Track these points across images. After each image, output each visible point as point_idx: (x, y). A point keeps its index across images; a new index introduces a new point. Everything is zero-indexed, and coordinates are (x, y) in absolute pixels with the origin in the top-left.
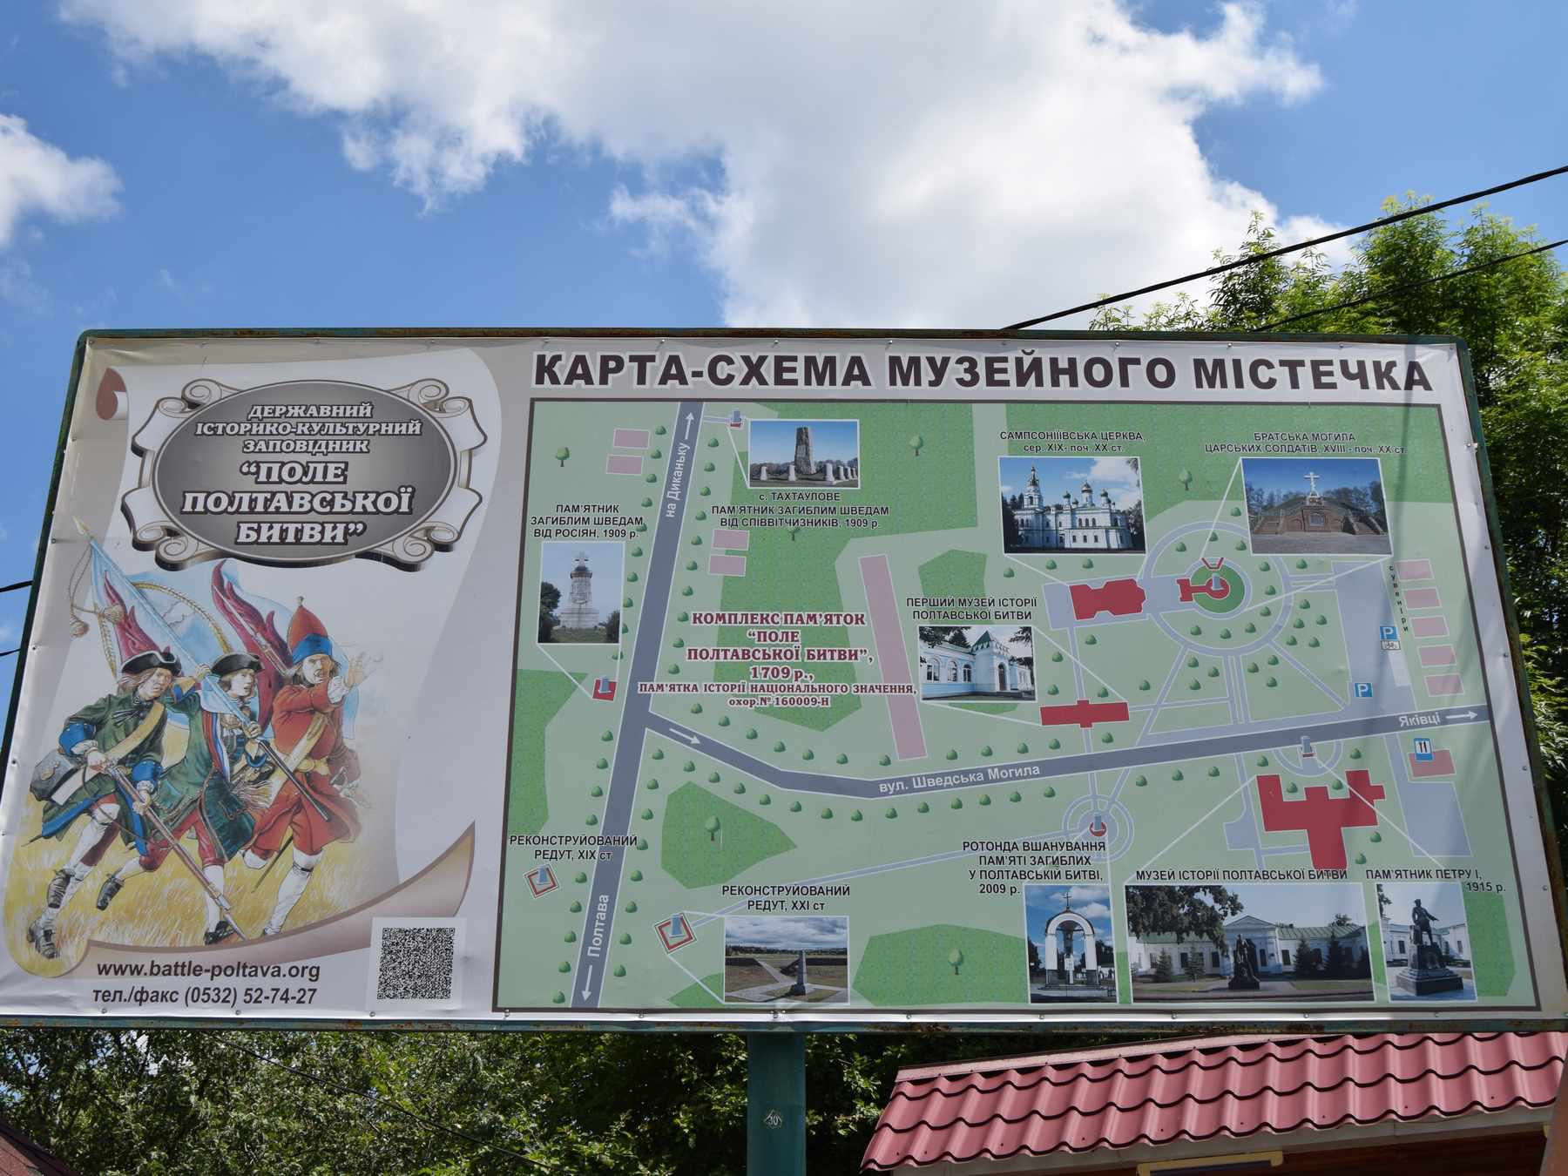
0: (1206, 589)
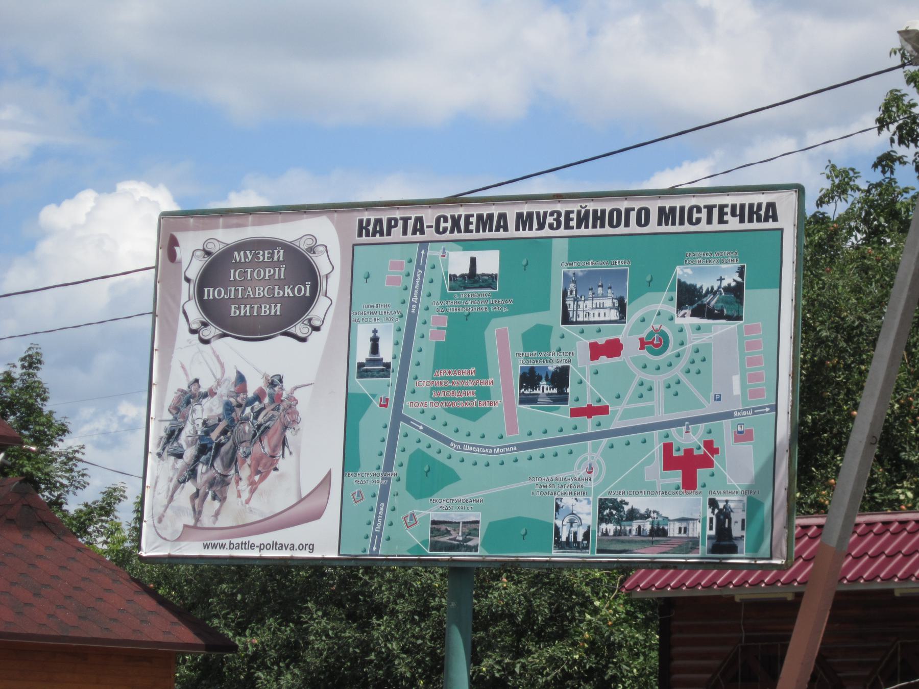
0: (652, 343)
